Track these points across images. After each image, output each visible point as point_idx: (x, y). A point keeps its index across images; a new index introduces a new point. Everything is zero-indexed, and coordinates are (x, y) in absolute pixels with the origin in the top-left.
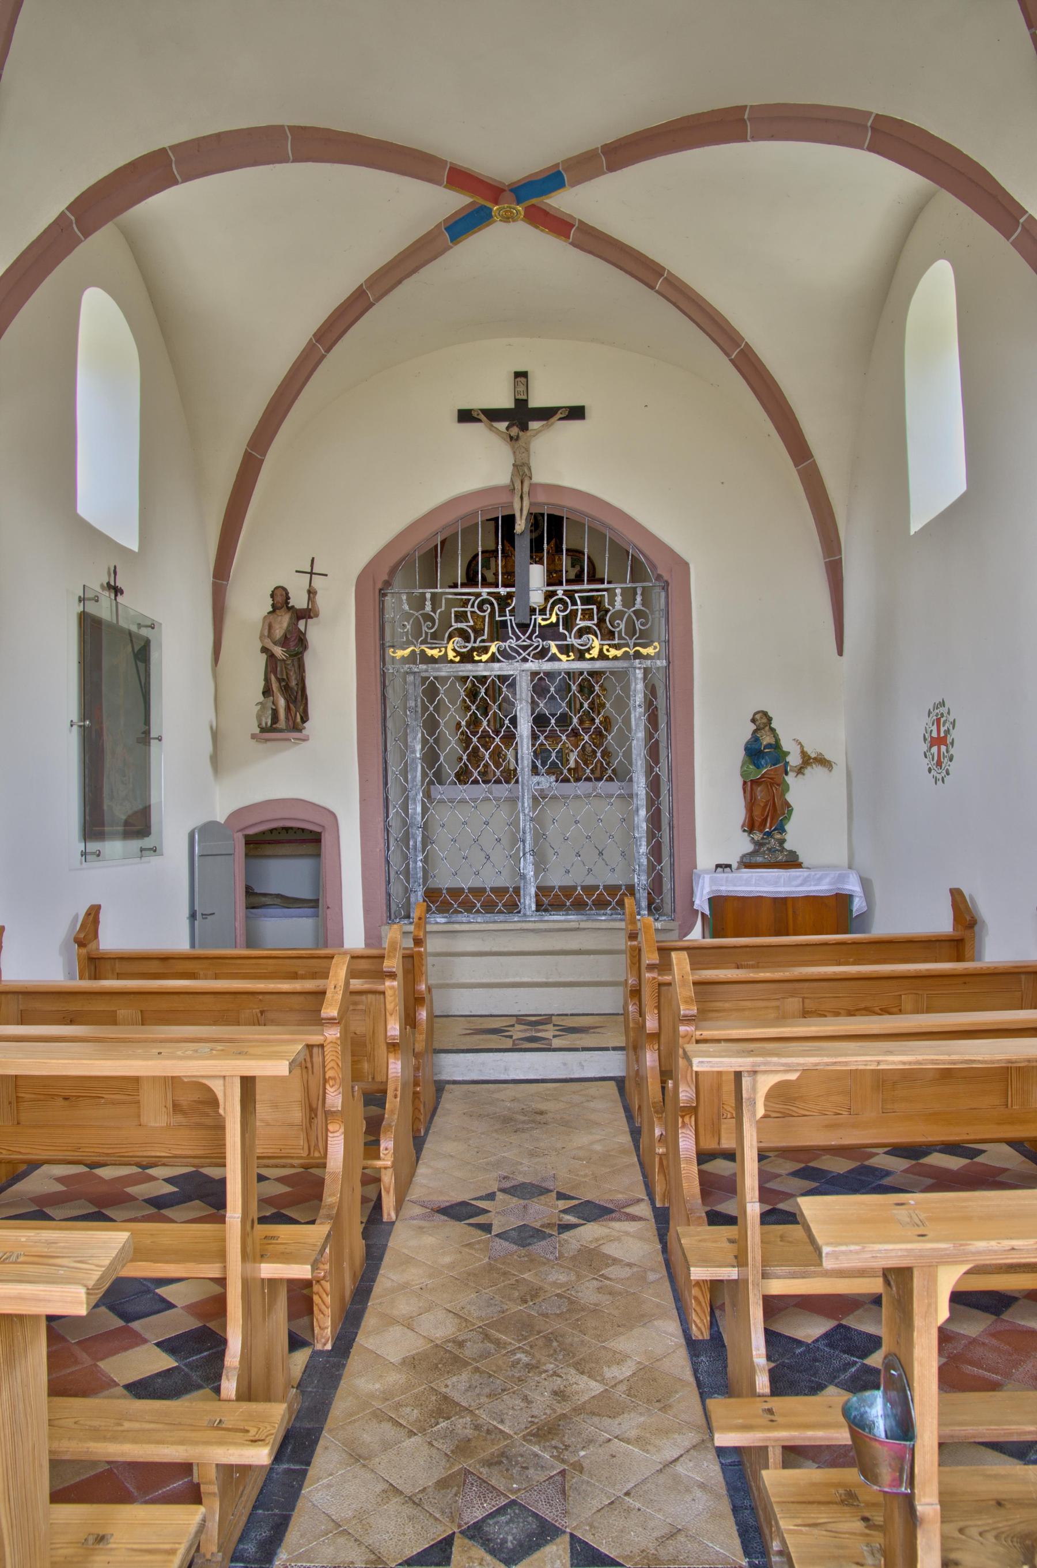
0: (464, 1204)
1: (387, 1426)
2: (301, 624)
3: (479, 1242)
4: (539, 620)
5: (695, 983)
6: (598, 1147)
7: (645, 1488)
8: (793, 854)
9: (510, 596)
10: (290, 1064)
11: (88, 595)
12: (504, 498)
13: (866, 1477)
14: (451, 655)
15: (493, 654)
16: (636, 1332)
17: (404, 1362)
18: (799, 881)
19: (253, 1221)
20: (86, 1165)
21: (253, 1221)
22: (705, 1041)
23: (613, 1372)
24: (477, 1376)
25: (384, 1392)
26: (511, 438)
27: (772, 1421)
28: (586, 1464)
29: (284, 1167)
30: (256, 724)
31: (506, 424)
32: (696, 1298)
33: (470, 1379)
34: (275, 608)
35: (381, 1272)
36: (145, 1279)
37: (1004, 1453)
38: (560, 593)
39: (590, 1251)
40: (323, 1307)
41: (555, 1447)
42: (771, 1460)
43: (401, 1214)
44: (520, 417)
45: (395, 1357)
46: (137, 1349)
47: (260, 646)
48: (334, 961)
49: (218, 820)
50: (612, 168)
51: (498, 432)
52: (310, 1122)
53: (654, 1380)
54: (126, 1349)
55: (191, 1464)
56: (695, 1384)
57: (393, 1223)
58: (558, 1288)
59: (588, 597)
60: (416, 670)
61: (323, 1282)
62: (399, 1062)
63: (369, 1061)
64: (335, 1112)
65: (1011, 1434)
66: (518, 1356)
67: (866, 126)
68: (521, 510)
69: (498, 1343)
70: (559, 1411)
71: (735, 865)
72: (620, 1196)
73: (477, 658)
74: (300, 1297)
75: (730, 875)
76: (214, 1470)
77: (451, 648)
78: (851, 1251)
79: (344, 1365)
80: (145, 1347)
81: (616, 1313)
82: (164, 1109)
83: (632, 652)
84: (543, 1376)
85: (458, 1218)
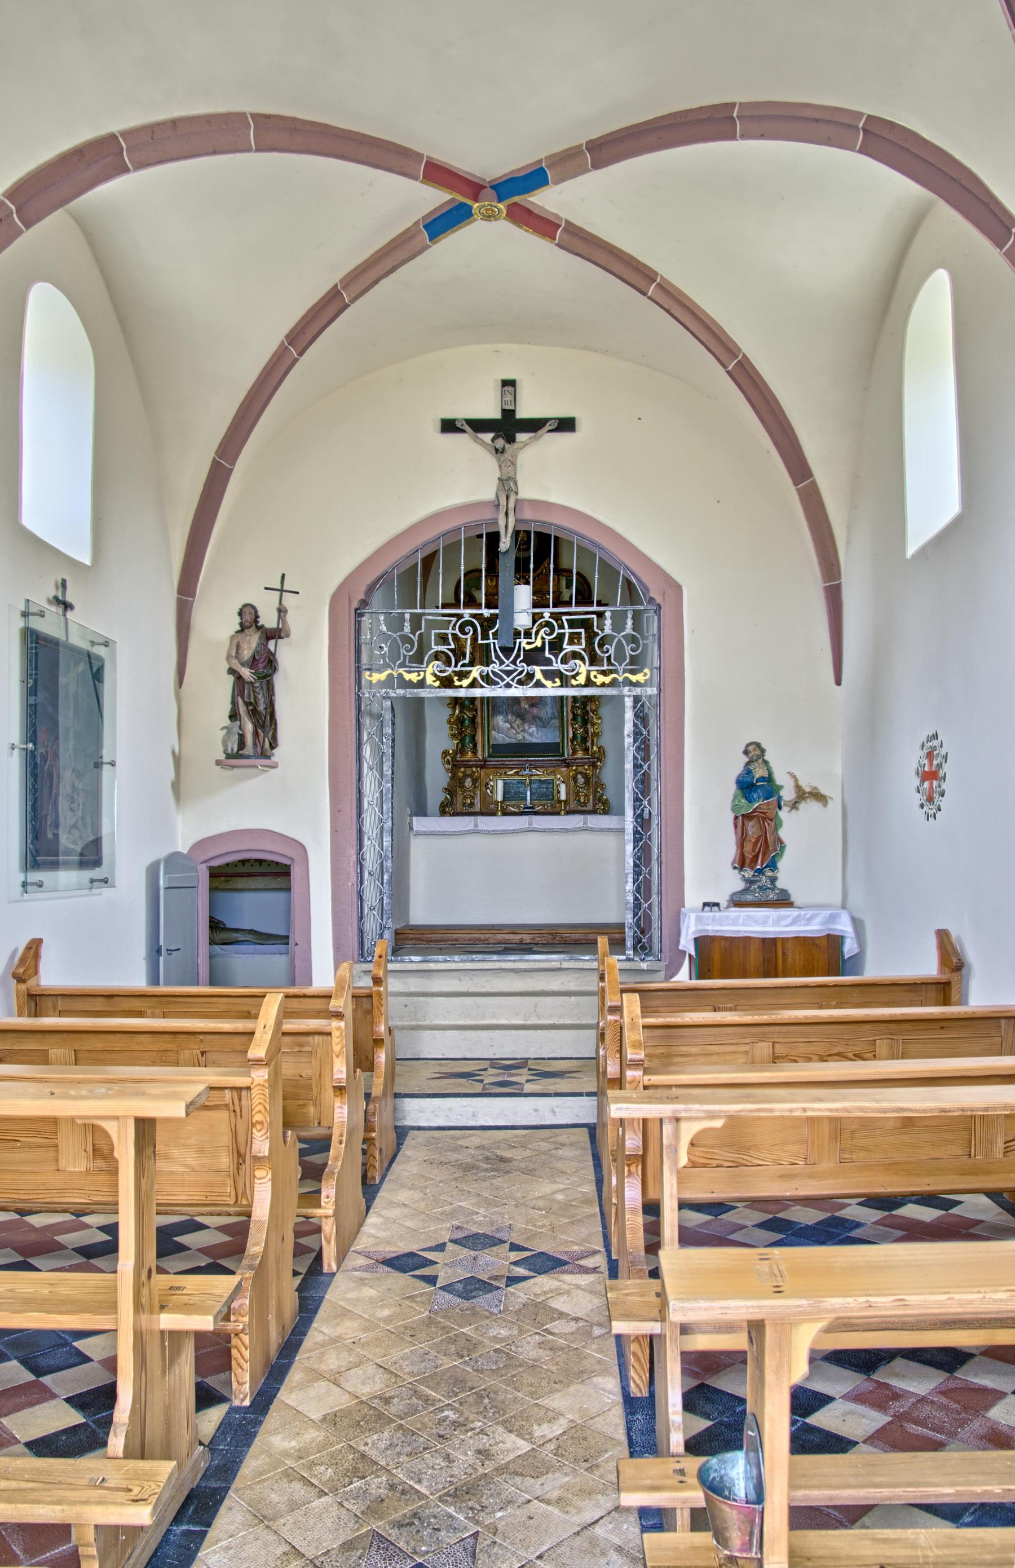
0: (411, 1255)
1: (297, 1485)
2: (271, 645)
3: (421, 1295)
4: (523, 645)
5: (644, 1027)
6: (560, 1197)
7: (559, 1551)
8: (784, 892)
9: (493, 618)
10: (188, 1107)
11: (33, 609)
12: (487, 515)
13: (718, 1542)
14: (430, 680)
15: (475, 679)
16: (572, 1389)
17: (324, 1419)
18: (789, 921)
19: (150, 1271)
20: (72, 1214)
21: (150, 1271)
22: (656, 1087)
23: (541, 1431)
24: (399, 1434)
25: (299, 1450)
26: (497, 450)
27: (681, 1482)
28: (501, 1526)
29: (219, 1215)
30: (221, 749)
31: (491, 435)
32: (635, 1354)
33: (392, 1437)
34: (243, 628)
35: (314, 1325)
36: (63, 1332)
37: (938, 1516)
38: (547, 615)
39: (536, 1305)
40: (242, 1361)
41: (471, 1508)
42: (679, 1523)
43: (343, 1265)
44: (507, 427)
45: (316, 1416)
46: (45, 1404)
47: (227, 667)
48: (266, 999)
49: (180, 850)
50: (596, 166)
51: (483, 443)
52: (238, 1169)
53: (585, 1439)
54: (32, 1404)
55: (69, 1526)
56: (626, 1444)
57: (334, 1274)
58: (498, 1343)
59: (583, 619)
60: (393, 695)
61: (241, 1335)
62: (346, 1107)
63: (315, 1105)
64: (261, 1158)
65: (929, 1496)
66: (446, 1413)
67: (857, 127)
68: (506, 527)
69: (427, 1400)
70: (481, 1471)
71: (723, 904)
72: (576, 1248)
73: (457, 683)
74: (214, 1352)
75: (718, 914)
76: (92, 1530)
77: (431, 671)
78: (699, 1308)
79: (261, 1422)
80: (53, 1402)
81: (554, 1369)
82: (84, 1153)
83: (621, 679)
84: (469, 1434)
85: (403, 1270)
